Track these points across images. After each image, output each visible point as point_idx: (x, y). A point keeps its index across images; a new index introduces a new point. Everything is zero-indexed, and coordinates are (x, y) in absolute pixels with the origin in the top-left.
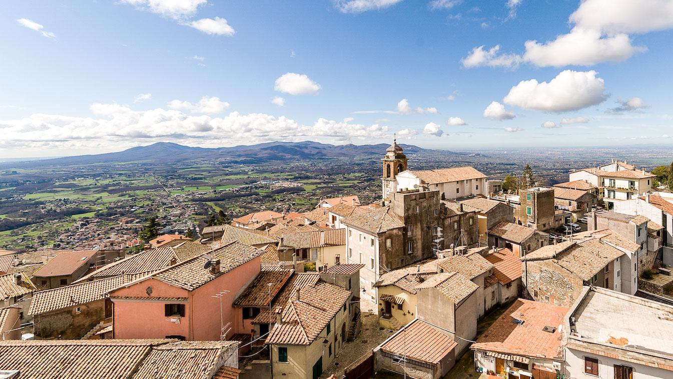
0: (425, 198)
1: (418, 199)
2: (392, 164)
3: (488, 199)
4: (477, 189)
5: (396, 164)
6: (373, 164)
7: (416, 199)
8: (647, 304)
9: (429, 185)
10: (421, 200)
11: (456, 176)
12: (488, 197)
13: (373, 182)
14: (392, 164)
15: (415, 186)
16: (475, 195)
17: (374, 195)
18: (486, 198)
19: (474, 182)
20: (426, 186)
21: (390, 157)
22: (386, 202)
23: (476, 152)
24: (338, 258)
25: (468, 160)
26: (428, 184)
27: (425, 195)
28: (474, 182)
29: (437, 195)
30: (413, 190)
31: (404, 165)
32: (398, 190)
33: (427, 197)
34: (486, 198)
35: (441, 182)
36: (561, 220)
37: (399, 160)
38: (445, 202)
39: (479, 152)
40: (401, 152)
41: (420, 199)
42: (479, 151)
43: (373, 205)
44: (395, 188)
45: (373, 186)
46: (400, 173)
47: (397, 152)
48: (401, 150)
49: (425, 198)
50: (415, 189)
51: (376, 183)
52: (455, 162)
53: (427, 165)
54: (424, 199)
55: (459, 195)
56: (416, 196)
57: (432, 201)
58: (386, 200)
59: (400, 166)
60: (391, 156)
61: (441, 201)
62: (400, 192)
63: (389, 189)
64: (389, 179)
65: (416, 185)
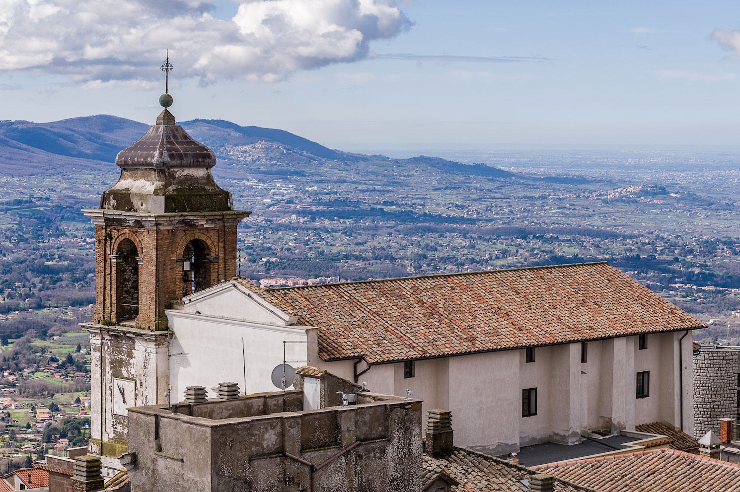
0: (336, 442)
1: (293, 448)
2: (147, 244)
3: (703, 459)
4: (642, 392)
5: (173, 243)
6: (38, 237)
7: (280, 452)
8: (47, 154)
9: (363, 366)
10: (314, 457)
11: (521, 316)
12: (706, 439)
13: (38, 343)
14: (147, 244)
15: (281, 373)
16: (631, 429)
17: (43, 413)
18: (694, 448)
19: (622, 351)
20: (342, 372)
21: (136, 202)
22: (105, 460)
23: (648, 177)
24: (167, 101)
25: (597, 222)
26: (361, 358)
27: (336, 427)
28: (622, 351)
29: (407, 429)
30: (265, 397)
31: (216, 250)
32: (179, 397)
33: (348, 436)
34: (694, 448)
35: (432, 351)
36: (124, 199)
37: (190, 216)
38: (454, 470)
39: (664, 177)
40: (200, 173)
41: (303, 450)
42: (669, 168)
43: (36, 475)
44: (164, 380)
45: (37, 365)
46: (194, 296)
47: (180, 173)
48: (204, 158)
49: (336, 442)
50: (277, 390)
51: (58, 347)
52: (524, 234)
53: (357, 250)
54: (332, 452)
55: (535, 428)
56: (282, 435)
57: (374, 464)
58: (112, 453)
59: (198, 249)
60: (143, 197)
61: (433, 465)
62: (188, 409)
63: (129, 386)
64: (129, 327)
65: (285, 366)
